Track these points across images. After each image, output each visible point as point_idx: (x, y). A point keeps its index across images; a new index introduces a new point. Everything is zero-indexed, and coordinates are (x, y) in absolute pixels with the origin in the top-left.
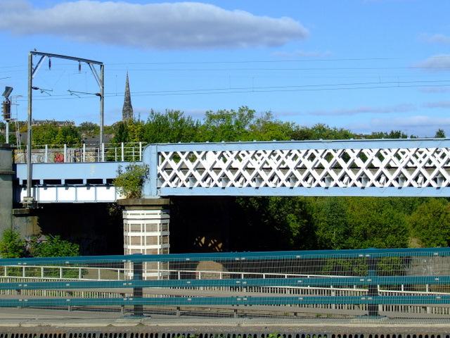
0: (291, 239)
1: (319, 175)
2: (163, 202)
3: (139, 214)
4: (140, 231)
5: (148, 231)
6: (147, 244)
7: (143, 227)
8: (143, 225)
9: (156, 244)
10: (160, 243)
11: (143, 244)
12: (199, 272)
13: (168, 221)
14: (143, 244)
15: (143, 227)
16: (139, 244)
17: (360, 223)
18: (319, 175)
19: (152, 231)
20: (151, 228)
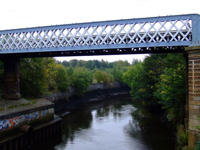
1: (185, 35)
18: (185, 35)
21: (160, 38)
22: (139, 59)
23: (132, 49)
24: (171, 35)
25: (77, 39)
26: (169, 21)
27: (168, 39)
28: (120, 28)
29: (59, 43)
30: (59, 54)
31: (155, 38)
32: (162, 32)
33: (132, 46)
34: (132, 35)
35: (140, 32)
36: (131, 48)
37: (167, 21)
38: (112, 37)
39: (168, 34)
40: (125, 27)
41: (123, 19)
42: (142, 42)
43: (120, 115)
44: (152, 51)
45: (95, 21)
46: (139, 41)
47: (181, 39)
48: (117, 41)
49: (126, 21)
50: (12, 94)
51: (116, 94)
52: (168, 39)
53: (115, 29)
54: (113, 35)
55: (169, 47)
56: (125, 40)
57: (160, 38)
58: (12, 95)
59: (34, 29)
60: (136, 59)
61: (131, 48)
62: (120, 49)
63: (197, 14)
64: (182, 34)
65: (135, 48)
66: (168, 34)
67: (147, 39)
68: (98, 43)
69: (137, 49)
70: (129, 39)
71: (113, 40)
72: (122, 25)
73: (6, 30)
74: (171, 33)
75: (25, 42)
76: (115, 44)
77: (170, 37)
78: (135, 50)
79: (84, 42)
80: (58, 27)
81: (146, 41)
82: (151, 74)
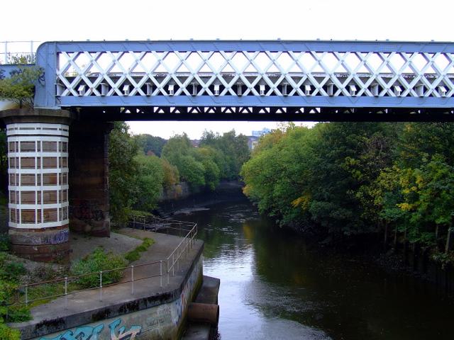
0: (426, 220)
1: (342, 83)
2: (66, 114)
3: (34, 129)
4: (34, 150)
5: (45, 202)
6: (44, 167)
7: (39, 146)
8: (39, 142)
9: (55, 167)
10: (60, 167)
11: (39, 167)
12: (142, 242)
13: (66, 140)
14: (39, 167)
15: (39, 146)
16: (33, 202)
17: (303, 145)
18: (342, 83)
19: (50, 150)
20: (49, 146)
21: (177, 87)
22: (214, 133)
23: (156, 109)
24: (246, 82)
25: (431, 80)
26: (218, 52)
27: (240, 91)
28: (134, 60)
29: (66, 88)
30: (147, 114)
31: (257, 88)
32: (135, 75)
33: (156, 104)
34: (160, 78)
35: (178, 71)
36: (152, 107)
37: (147, 52)
38: (115, 79)
39: (194, 79)
40: (121, 59)
41: (391, 39)
42: (183, 94)
43: (243, 253)
44: (327, 114)
45: (91, 40)
46: (130, 92)
47: (266, 92)
48: (126, 88)
49: (422, 46)
50: (97, 220)
51: (187, 212)
52: (240, 91)
53: (98, 61)
54: (118, 75)
55: (237, 108)
56: (99, 89)
57: (177, 87)
58: (97, 222)
59: (171, 45)
60: (209, 131)
61: (152, 107)
62: (127, 108)
63: (42, 45)
64: (360, 82)
65: (160, 108)
66: (194, 79)
67: (148, 87)
68: (78, 92)
69: (166, 109)
70: (199, 88)
71: (160, 86)
72: (115, 52)
73: (276, 39)
74: (247, 77)
75: (390, 79)
76: (76, 97)
77: (244, 88)
78: (161, 111)
79: (87, 88)
80: (334, 45)
81: (191, 92)
82: (352, 167)
